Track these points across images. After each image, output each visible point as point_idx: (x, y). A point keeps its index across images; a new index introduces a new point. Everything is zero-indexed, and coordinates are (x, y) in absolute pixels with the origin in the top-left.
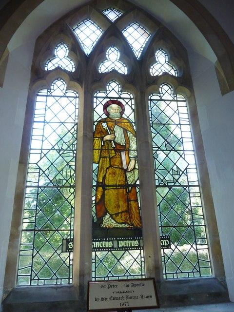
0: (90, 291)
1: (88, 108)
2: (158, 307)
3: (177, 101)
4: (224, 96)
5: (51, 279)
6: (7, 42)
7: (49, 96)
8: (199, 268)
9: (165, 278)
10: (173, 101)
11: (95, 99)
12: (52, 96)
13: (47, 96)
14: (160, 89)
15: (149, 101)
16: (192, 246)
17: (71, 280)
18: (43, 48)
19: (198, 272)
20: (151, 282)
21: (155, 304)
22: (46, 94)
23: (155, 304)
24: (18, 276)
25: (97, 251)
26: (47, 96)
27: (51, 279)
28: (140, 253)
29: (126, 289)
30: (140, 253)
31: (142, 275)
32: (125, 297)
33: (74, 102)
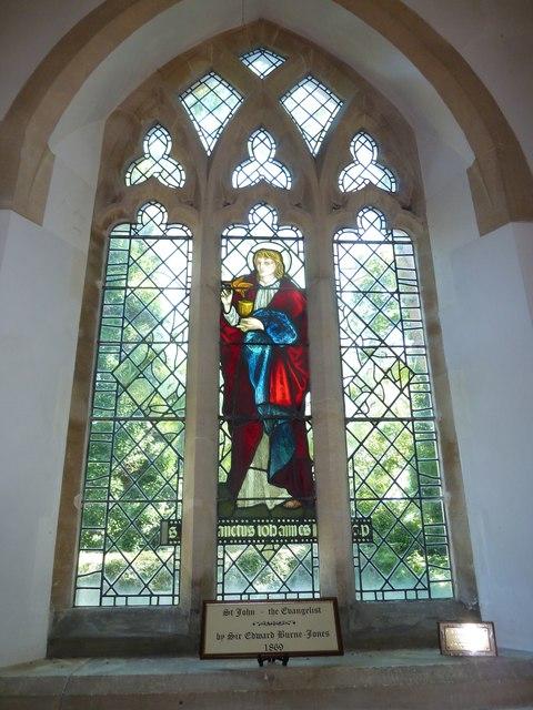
2: (340, 653)
10: (357, 242)
20: (329, 606)
21: (334, 646)
28: (311, 550)
30: (174, 554)
31: (361, 591)
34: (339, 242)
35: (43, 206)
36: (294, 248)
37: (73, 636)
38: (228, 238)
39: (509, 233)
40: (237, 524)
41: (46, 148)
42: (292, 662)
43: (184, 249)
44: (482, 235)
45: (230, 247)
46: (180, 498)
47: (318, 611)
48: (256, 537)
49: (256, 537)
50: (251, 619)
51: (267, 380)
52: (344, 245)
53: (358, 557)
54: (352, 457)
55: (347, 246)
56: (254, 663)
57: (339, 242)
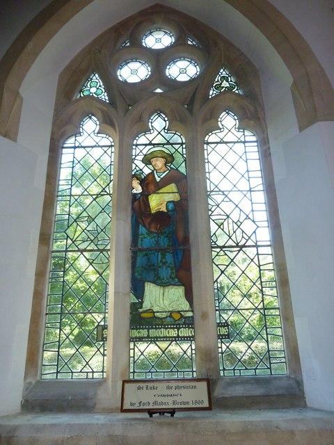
0: (125, 389)
1: (124, 158)
2: (209, 409)
3: (245, 142)
4: (306, 131)
5: (171, 371)
6: (185, 82)
7: (78, 147)
8: (270, 363)
9: (222, 374)
10: (237, 142)
11: (205, 146)
12: (82, 147)
13: (75, 147)
14: (150, 124)
15: (184, 142)
16: (98, 350)
17: (194, 373)
18: (72, 80)
19: (268, 368)
20: (204, 384)
21: (206, 404)
22: (73, 145)
23: (206, 404)
24: (42, 374)
25: (223, 338)
26: (75, 147)
27: (171, 371)
28: (191, 345)
29: (169, 392)
30: (191, 345)
31: (224, 369)
32: (151, 404)
33: (109, 152)
34: (208, 143)
35: (16, 134)
36: (180, 150)
37: (42, 400)
38: (137, 145)
39: (320, 129)
40: (160, 328)
41: (18, 92)
42: (176, 415)
43: (109, 152)
44: (301, 129)
45: (138, 151)
46: (218, 312)
47: (195, 387)
48: (178, 336)
49: (178, 336)
50: (154, 392)
51: (165, 238)
52: (211, 145)
53: (134, 349)
54: (216, 281)
55: (213, 146)
56: (146, 415)
57: (208, 143)
